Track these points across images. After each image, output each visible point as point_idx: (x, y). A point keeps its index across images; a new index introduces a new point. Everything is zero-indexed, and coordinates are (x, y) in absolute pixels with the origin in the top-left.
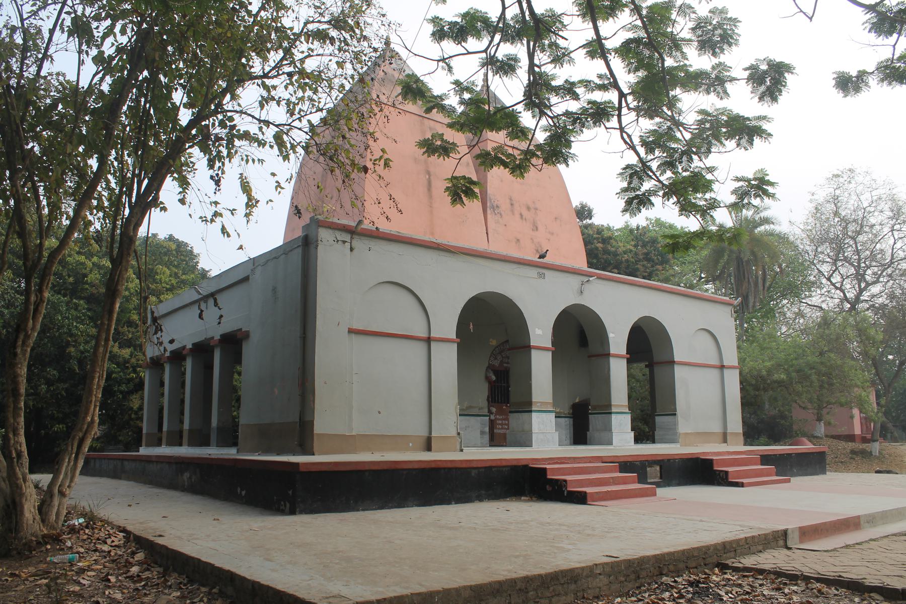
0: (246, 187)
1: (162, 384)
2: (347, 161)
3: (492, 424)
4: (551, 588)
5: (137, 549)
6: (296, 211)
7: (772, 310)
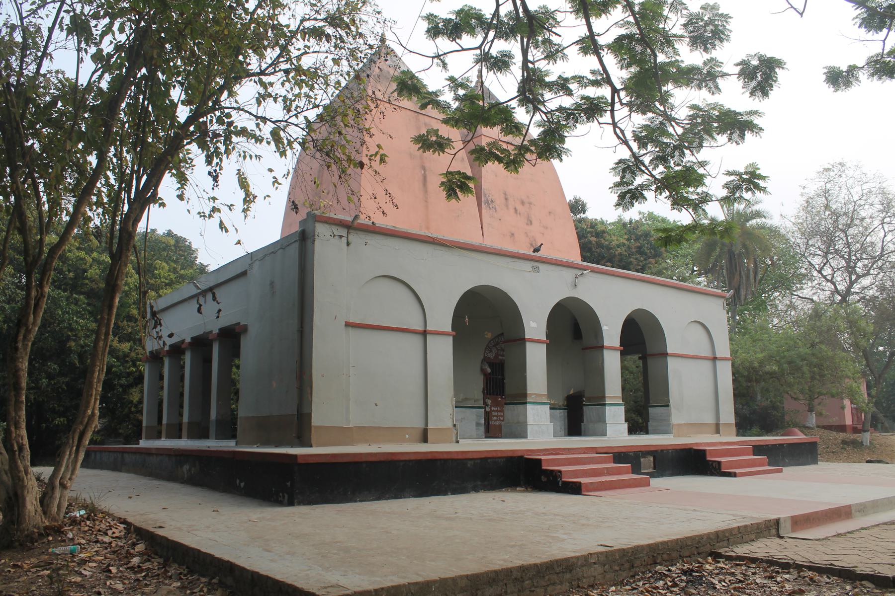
0: (243, 183)
1: (161, 378)
2: (344, 157)
3: (488, 416)
4: (547, 578)
5: (138, 540)
6: (293, 206)
7: (764, 302)
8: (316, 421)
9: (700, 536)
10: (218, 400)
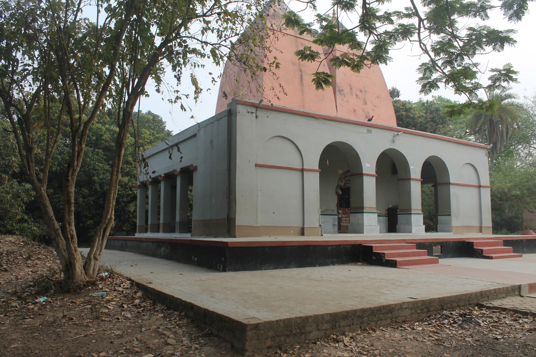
0: (194, 82)
2: (254, 65)
3: (340, 220)
4: (377, 316)
5: (138, 290)
6: (223, 94)
7: (512, 152)
8: (238, 222)
10: (180, 210)
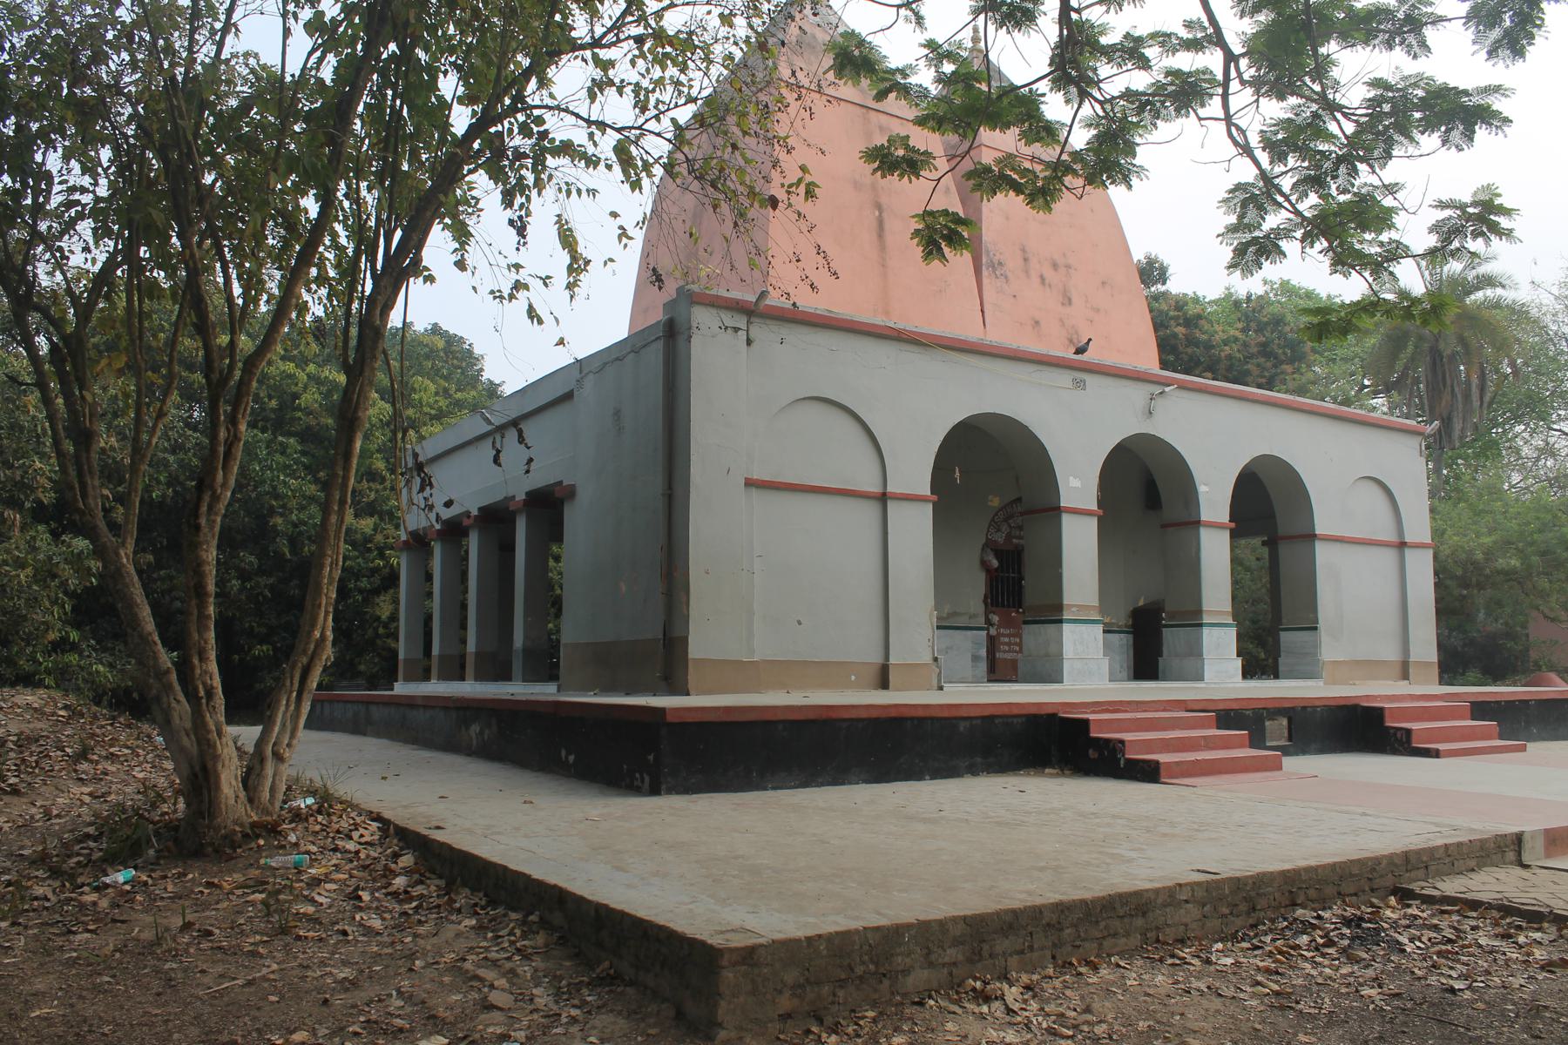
0: (567, 239)
1: (429, 577)
2: (741, 189)
3: (992, 643)
4: (1102, 924)
6: (652, 276)
8: (695, 651)
9: (1376, 858)
10: (526, 616)
